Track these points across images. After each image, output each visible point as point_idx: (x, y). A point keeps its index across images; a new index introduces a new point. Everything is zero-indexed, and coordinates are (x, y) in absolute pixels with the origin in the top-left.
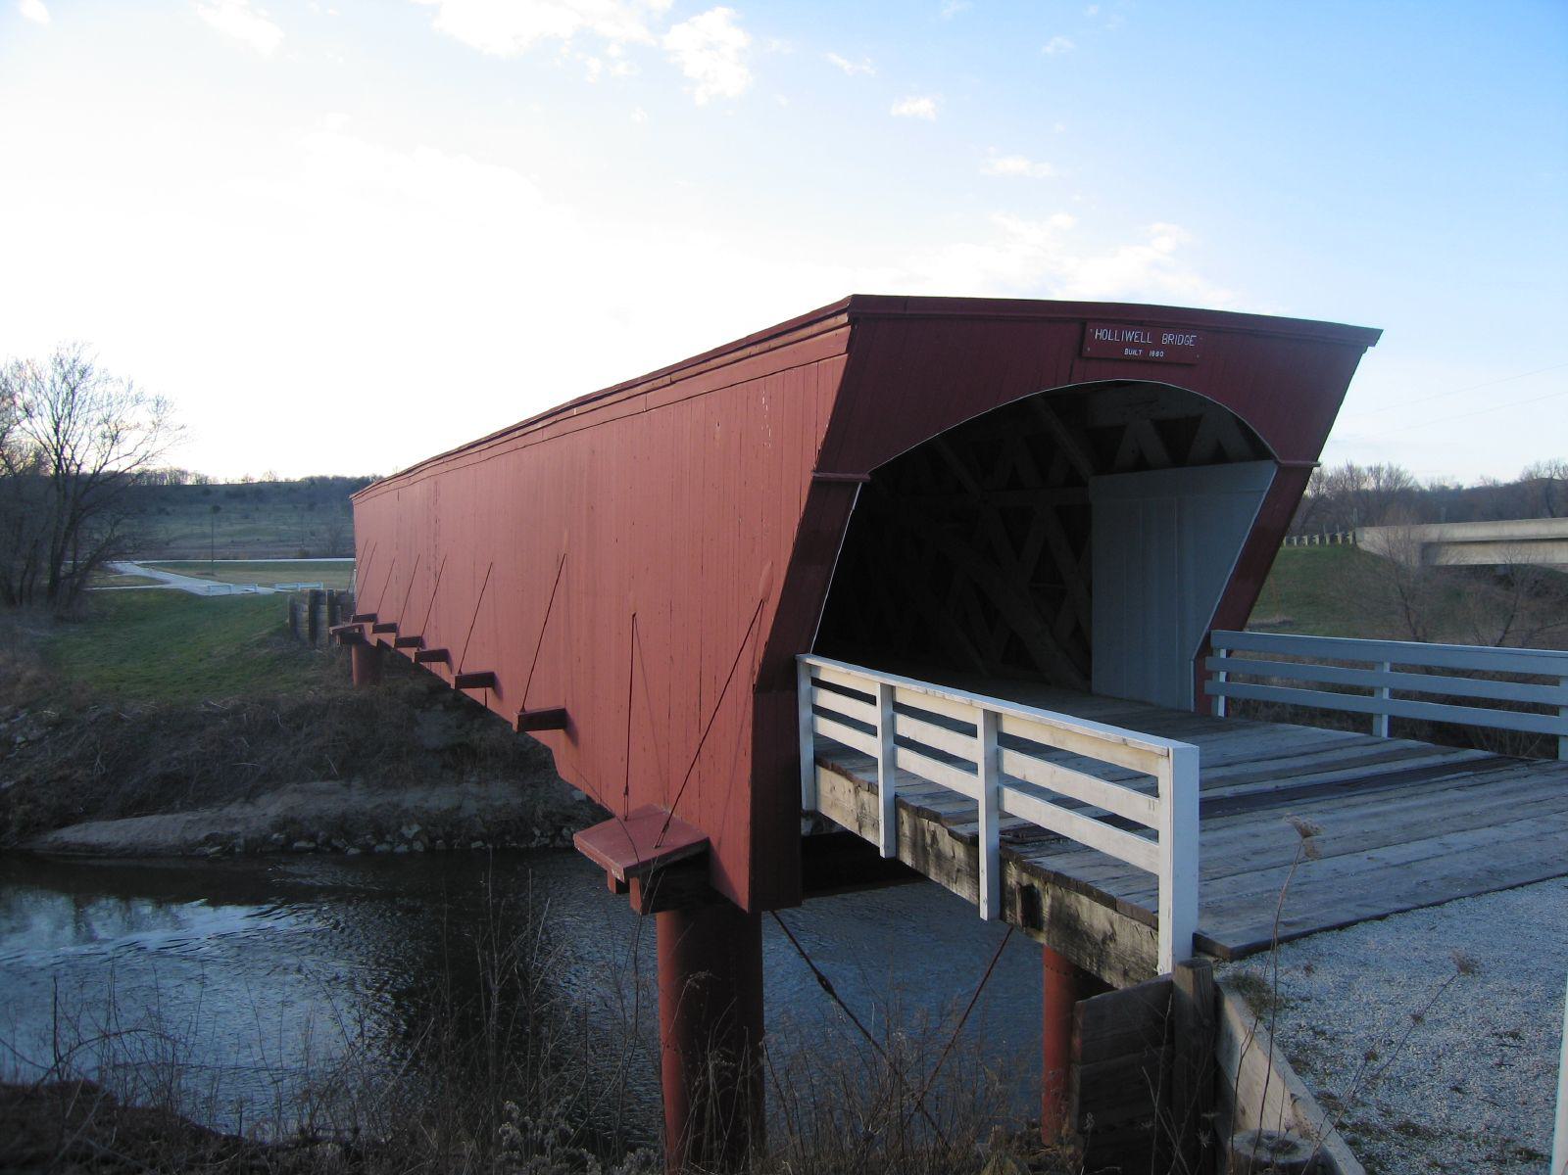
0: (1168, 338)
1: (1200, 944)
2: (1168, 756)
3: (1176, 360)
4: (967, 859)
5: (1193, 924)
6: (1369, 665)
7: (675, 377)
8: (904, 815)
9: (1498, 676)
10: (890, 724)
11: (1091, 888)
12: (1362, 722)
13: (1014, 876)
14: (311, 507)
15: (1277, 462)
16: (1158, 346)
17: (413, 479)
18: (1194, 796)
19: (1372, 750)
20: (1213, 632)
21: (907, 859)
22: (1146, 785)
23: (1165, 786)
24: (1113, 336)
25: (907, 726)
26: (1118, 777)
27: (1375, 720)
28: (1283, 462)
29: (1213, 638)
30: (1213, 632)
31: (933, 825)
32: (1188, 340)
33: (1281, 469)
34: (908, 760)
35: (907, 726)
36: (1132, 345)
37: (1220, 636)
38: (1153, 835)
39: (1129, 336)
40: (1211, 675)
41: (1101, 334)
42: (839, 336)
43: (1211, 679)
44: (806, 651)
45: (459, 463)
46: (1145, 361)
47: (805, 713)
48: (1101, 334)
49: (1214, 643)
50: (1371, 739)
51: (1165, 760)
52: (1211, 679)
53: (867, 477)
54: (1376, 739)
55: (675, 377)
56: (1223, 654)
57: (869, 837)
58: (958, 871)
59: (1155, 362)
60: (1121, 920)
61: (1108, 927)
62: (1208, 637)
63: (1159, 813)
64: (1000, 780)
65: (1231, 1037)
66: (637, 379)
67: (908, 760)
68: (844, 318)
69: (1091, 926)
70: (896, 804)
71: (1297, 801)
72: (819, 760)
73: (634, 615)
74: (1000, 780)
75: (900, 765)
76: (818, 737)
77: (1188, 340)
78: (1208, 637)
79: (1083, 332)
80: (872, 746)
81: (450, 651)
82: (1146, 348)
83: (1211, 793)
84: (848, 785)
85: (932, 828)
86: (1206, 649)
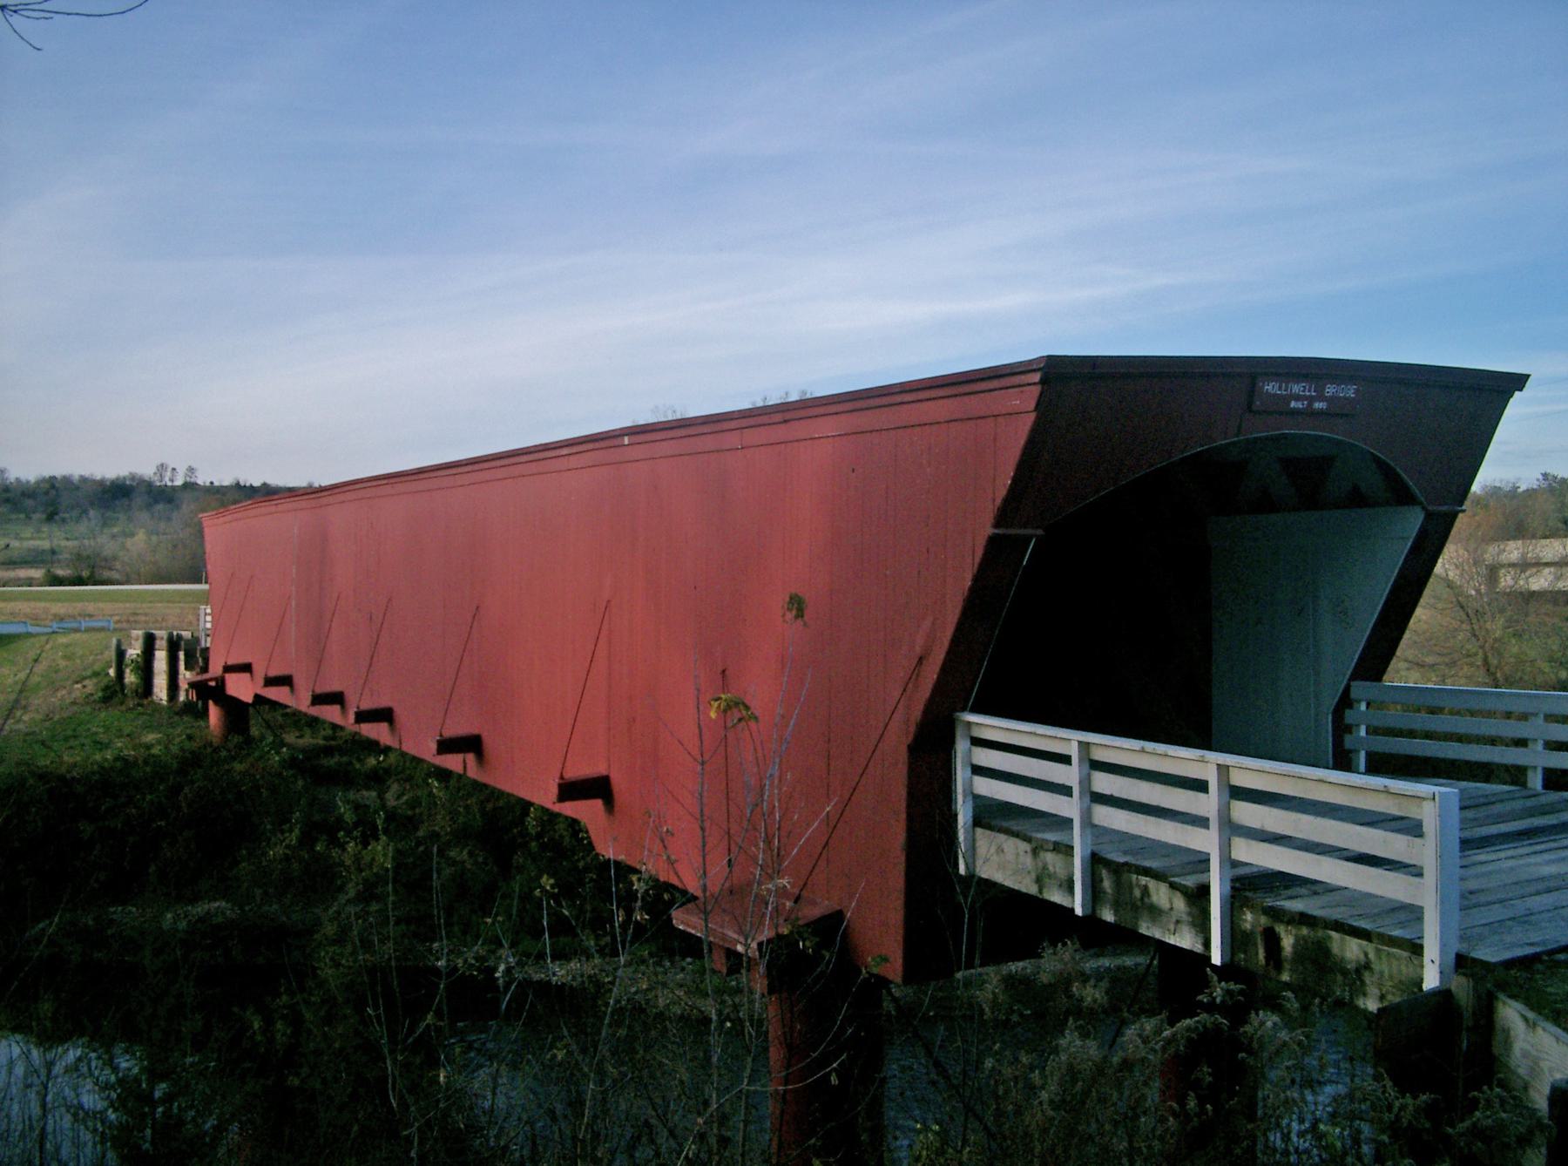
0: (1330, 390)
1: (1462, 962)
2: (1434, 799)
3: (1338, 412)
4: (1188, 909)
5: (1456, 947)
6: (1524, 717)
7: (788, 416)
8: (1104, 873)
9: (1381, 731)
10: (1086, 782)
11: (1343, 924)
12: (1516, 775)
13: (1248, 919)
14: (51, 518)
15: (1424, 508)
16: (1321, 398)
17: (325, 501)
18: (1455, 836)
19: (1529, 803)
20: (1352, 683)
21: (1108, 916)
22: (1414, 829)
23: (1430, 826)
24: (1280, 388)
25: (1104, 783)
26: (1367, 820)
27: (1530, 774)
28: (1430, 508)
29: (1352, 689)
30: (1352, 683)
31: (1144, 880)
32: (1350, 392)
33: (1429, 516)
34: (1107, 816)
35: (1104, 783)
36: (1298, 398)
37: (1360, 689)
38: (1419, 873)
39: (1296, 388)
40: (1349, 729)
41: (1270, 387)
42: (1024, 401)
43: (1351, 733)
44: (963, 710)
45: (421, 485)
46: (1312, 414)
47: (961, 774)
48: (1270, 387)
49: (1353, 695)
50: (1525, 793)
51: (1432, 803)
52: (1351, 733)
53: (1040, 532)
54: (1531, 792)
55: (788, 416)
56: (1363, 707)
57: (1056, 897)
58: (1178, 922)
59: (1321, 413)
60: (1378, 951)
61: (1362, 957)
62: (1347, 690)
63: (1425, 852)
64: (1231, 829)
65: (1506, 1031)
66: (733, 412)
67: (1107, 816)
68: (1037, 377)
69: (1343, 958)
70: (1095, 861)
71: (1488, 849)
72: (978, 822)
73: (724, 671)
74: (1231, 829)
75: (1096, 821)
76: (976, 797)
77: (1350, 392)
78: (1347, 690)
79: (1254, 385)
80: (1068, 807)
81: (395, 709)
82: (1311, 400)
83: (1467, 834)
84: (1024, 846)
85: (1144, 883)
86: (1345, 702)
